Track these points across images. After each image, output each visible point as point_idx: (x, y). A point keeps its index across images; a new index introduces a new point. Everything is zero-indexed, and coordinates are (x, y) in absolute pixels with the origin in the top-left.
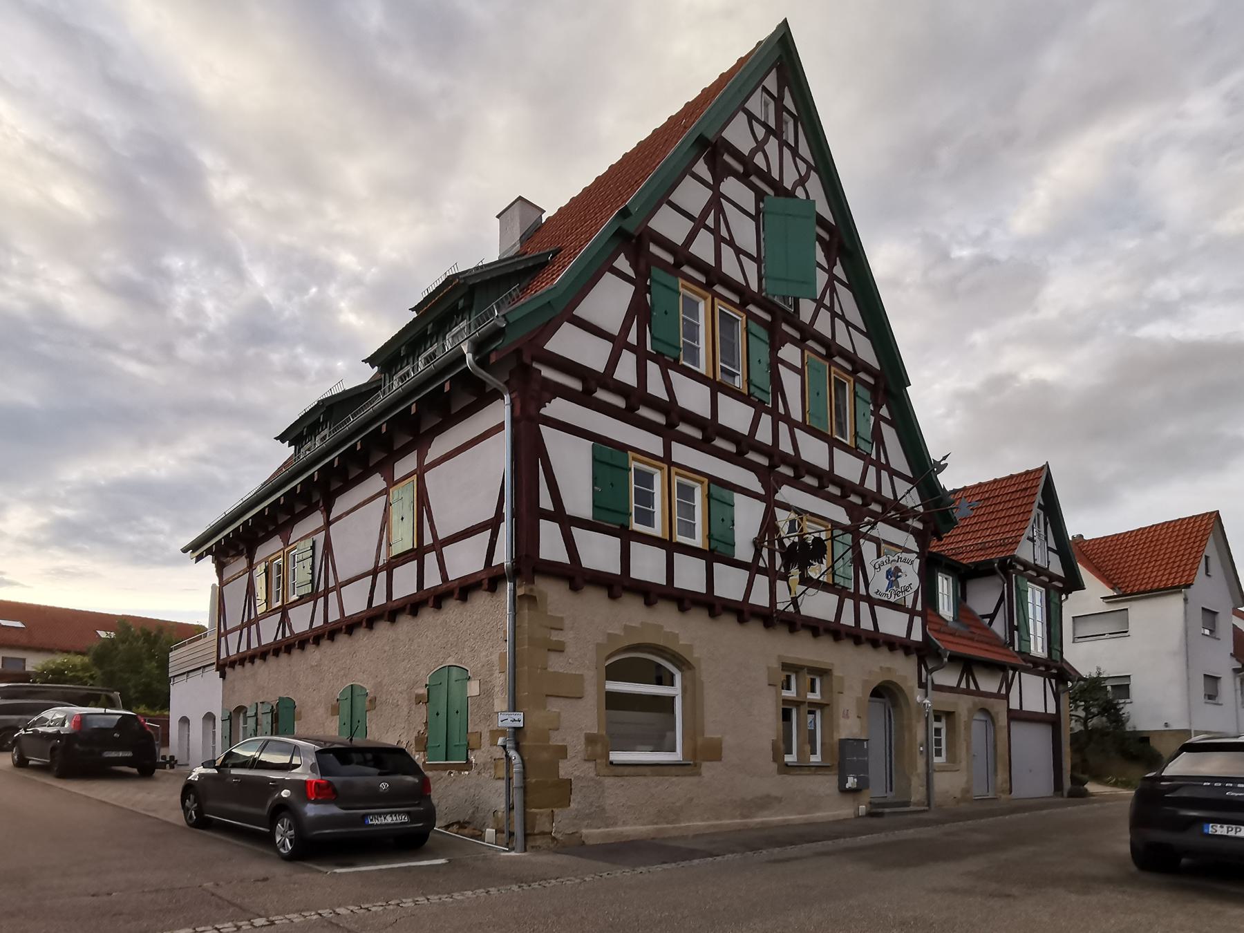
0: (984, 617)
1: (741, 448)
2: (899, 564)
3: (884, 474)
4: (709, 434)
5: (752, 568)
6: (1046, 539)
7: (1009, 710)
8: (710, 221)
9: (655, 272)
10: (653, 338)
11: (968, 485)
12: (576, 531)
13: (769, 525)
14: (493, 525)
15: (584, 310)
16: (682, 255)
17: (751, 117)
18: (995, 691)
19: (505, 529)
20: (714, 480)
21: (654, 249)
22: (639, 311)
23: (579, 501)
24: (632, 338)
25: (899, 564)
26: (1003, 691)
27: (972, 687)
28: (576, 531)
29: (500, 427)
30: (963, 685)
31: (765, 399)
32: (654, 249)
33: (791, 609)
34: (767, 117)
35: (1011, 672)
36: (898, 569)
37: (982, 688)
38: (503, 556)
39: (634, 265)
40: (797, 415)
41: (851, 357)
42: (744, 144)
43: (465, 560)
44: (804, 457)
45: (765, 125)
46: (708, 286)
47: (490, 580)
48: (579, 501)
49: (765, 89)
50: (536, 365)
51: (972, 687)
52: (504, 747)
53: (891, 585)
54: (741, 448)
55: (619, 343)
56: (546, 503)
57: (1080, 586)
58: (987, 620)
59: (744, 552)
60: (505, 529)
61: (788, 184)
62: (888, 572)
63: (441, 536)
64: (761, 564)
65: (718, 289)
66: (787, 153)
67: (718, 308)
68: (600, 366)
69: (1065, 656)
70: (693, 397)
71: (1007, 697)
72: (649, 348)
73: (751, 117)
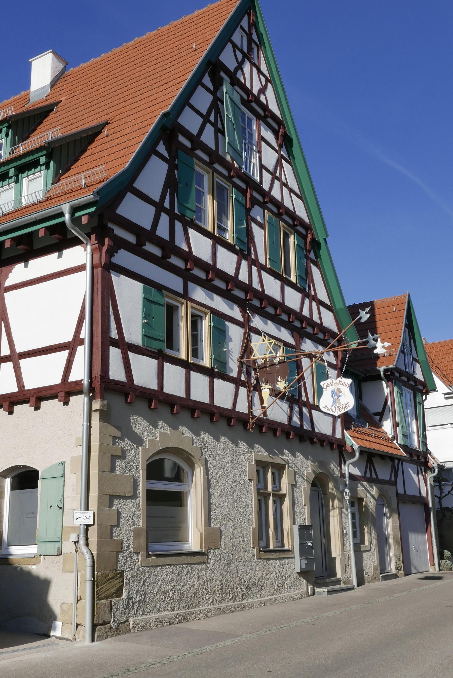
0: (376, 414)
1: (229, 287)
2: (340, 386)
3: (314, 304)
4: (212, 278)
5: (237, 382)
6: (411, 351)
7: (398, 495)
8: (212, 118)
9: (180, 153)
10: (179, 203)
11: (357, 303)
12: (131, 355)
13: (247, 349)
14: (71, 347)
15: (138, 185)
16: (195, 140)
17: (235, 46)
18: (388, 478)
19: (82, 353)
20: (215, 312)
21: (181, 139)
22: (171, 183)
23: (134, 333)
24: (167, 204)
25: (340, 386)
26: (393, 479)
27: (374, 476)
28: (131, 355)
29: (81, 268)
30: (368, 475)
31: (243, 249)
32: (181, 139)
33: (262, 416)
34: (242, 46)
35: (396, 461)
36: (339, 390)
37: (380, 477)
38: (79, 372)
39: (168, 150)
40: (262, 260)
41: (292, 215)
42: (231, 65)
43: (43, 373)
44: (266, 292)
45: (241, 51)
46: (210, 164)
47: (65, 391)
48: (134, 333)
49: (242, 28)
50: (110, 225)
51: (374, 476)
52: (76, 543)
53: (335, 402)
54: (229, 287)
55: (159, 207)
56: (114, 334)
57: (434, 389)
58: (378, 417)
59: (233, 368)
60: (82, 353)
61: (255, 92)
62: (333, 392)
63: (19, 349)
64: (243, 378)
65: (217, 166)
66: (254, 70)
67: (216, 180)
68: (147, 225)
69: (429, 448)
70: (200, 246)
71: (395, 484)
72: (176, 211)
73: (235, 46)
